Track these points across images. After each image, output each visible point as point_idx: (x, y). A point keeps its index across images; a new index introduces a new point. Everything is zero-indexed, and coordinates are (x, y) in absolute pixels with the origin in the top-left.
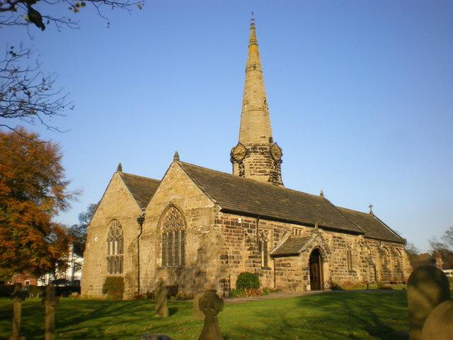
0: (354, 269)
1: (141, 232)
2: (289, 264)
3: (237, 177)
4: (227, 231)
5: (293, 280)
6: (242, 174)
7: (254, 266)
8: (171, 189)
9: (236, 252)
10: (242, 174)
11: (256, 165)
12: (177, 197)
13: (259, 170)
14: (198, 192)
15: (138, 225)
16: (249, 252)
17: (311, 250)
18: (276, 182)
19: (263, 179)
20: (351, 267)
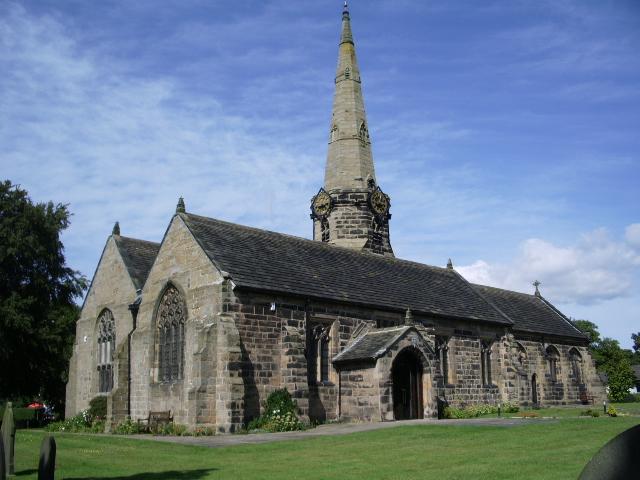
0: (494, 382)
1: (135, 328)
2: (360, 376)
3: (319, 243)
4: (247, 323)
5: (366, 403)
6: (326, 237)
7: (295, 380)
8: (171, 257)
9: (264, 358)
10: (326, 237)
11: (346, 222)
12: (179, 270)
13: (350, 229)
14: (205, 260)
15: (129, 314)
16: (287, 358)
17: (395, 353)
18: (379, 249)
19: (357, 244)
20: (490, 379)
